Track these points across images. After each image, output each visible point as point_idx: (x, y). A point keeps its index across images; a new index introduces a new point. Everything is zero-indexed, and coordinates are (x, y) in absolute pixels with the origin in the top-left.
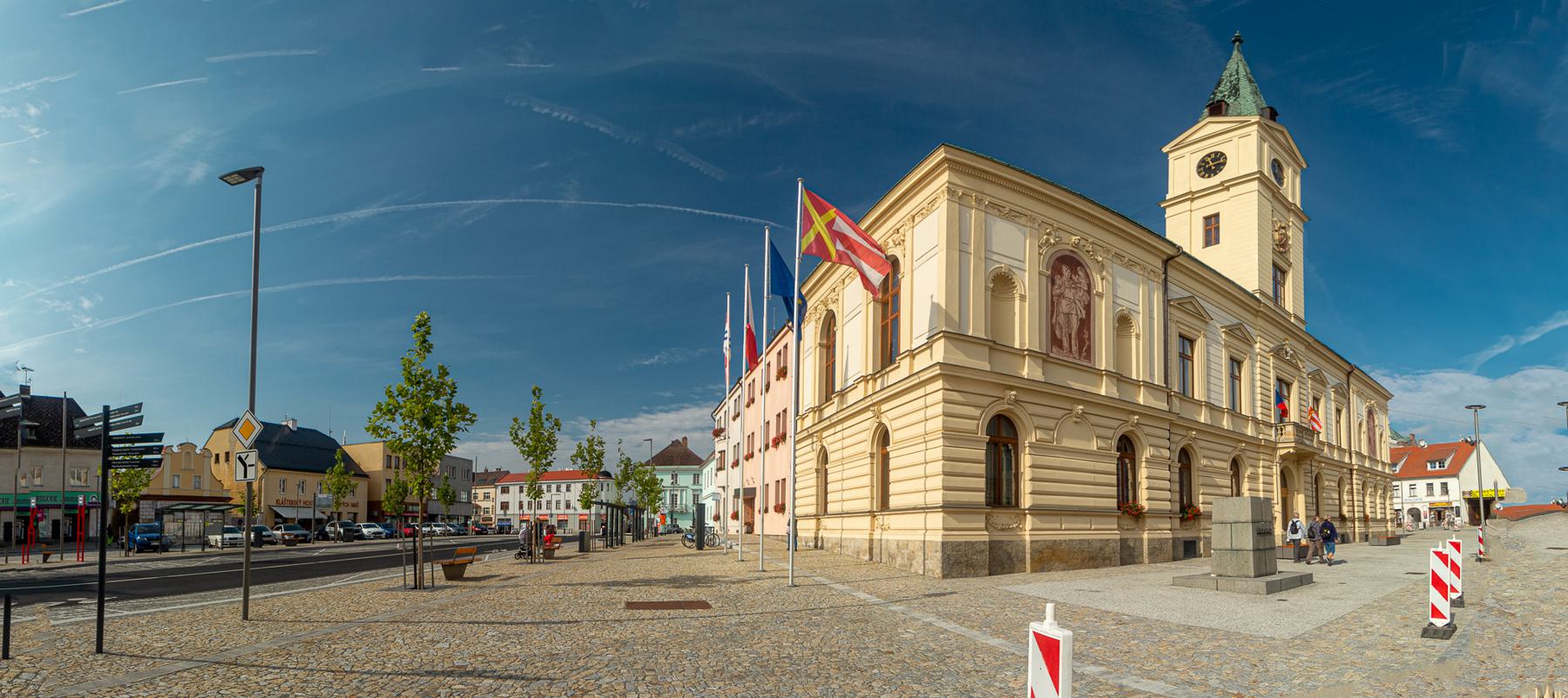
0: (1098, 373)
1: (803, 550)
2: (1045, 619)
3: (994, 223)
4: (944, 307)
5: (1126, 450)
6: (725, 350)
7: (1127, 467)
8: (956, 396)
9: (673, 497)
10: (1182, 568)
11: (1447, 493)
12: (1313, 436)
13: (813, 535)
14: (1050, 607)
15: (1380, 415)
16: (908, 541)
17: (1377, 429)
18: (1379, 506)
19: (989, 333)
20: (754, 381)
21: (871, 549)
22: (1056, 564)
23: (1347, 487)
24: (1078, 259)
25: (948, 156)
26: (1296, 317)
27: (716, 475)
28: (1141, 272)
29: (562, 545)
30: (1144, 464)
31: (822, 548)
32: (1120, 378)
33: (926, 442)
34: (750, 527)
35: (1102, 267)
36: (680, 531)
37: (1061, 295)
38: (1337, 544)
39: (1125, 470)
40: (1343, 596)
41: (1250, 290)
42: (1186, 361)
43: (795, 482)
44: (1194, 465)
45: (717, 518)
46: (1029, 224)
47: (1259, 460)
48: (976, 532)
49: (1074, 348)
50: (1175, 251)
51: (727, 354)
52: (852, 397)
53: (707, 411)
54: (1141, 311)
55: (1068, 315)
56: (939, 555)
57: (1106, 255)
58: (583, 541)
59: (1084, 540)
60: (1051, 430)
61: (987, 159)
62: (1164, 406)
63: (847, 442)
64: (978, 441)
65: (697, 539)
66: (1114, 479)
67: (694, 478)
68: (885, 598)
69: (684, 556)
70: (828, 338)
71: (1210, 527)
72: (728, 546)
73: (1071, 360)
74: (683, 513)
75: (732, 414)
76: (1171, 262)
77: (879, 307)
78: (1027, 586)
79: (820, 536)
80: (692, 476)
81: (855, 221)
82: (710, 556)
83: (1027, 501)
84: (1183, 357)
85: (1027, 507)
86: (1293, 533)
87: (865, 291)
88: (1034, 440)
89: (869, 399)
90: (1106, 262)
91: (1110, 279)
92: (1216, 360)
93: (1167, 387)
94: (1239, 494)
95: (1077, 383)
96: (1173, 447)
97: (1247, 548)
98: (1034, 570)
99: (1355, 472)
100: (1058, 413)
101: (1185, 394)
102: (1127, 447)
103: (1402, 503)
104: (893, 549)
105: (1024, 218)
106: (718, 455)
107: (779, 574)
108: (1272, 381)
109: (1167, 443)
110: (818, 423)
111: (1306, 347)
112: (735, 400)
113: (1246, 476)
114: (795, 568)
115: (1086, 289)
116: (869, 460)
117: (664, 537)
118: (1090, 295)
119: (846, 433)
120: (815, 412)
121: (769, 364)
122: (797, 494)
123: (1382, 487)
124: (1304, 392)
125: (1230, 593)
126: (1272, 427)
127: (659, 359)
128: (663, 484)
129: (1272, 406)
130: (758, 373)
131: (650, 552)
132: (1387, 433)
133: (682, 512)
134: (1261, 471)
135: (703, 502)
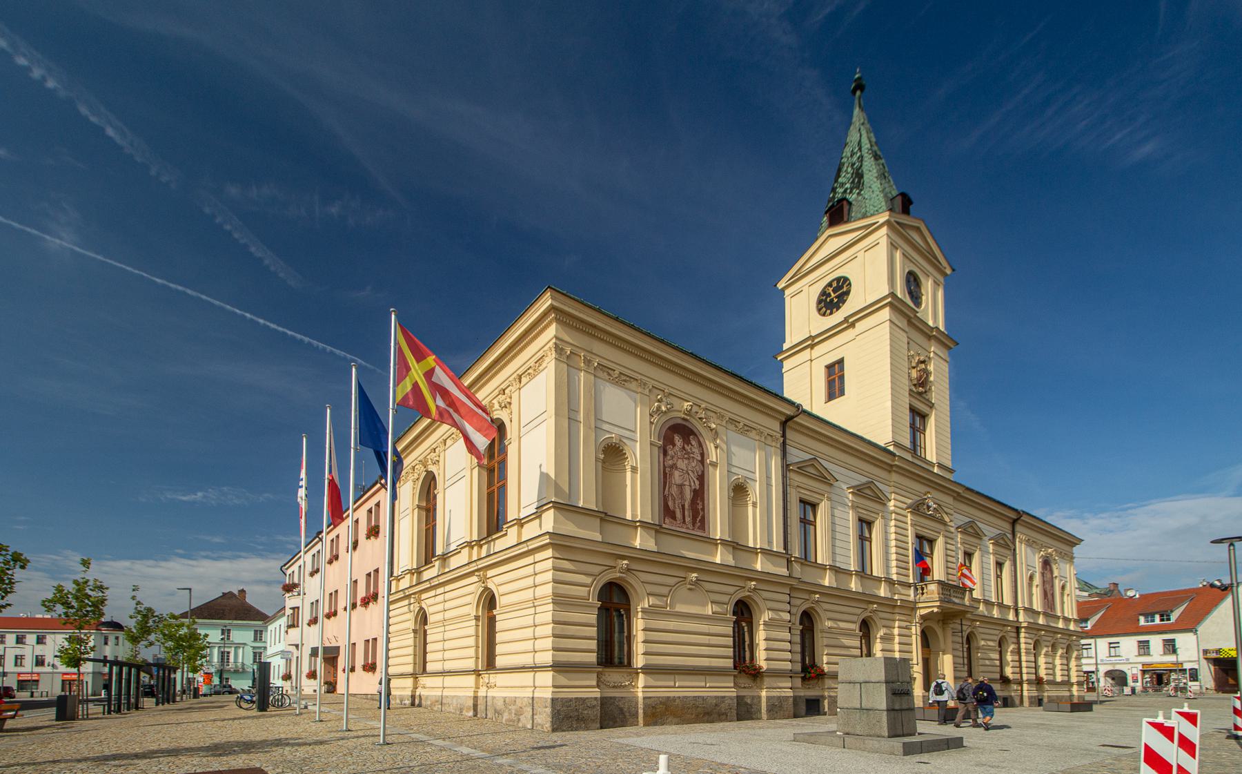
0: (714, 543)
1: (395, 708)
2: (658, 769)
3: (604, 389)
4: (553, 477)
5: (742, 614)
6: (299, 500)
7: (743, 630)
8: (567, 565)
9: (224, 656)
10: (803, 725)
11: (1174, 651)
12: (964, 594)
13: (410, 694)
14: (663, 759)
15: (1061, 564)
16: (516, 698)
17: (1057, 582)
18: (1058, 668)
19: (600, 504)
20: (338, 536)
21: (475, 707)
22: (670, 719)
23: (1012, 647)
24: (690, 426)
25: (555, 304)
26: (940, 466)
27: (287, 632)
28: (757, 438)
29: (20, 713)
30: (762, 627)
31: (420, 705)
32: (736, 546)
33: (535, 607)
34: (331, 687)
35: (715, 434)
36: (232, 691)
37: (674, 467)
38: (997, 707)
39: (741, 633)
40: (1004, 765)
41: (882, 444)
42: (807, 526)
43: (388, 641)
44: (818, 627)
45: (287, 677)
46: (640, 390)
47: (894, 620)
48: (587, 689)
49: (688, 519)
50: (794, 409)
51: (303, 504)
52: (455, 562)
53: (274, 564)
54: (758, 479)
55: (681, 486)
56: (549, 710)
57: (719, 422)
58: (65, 709)
59: (699, 697)
60: (664, 596)
61: (594, 309)
62: (783, 571)
63: (448, 605)
64: (591, 606)
65: (259, 700)
66: (730, 641)
67: (255, 634)
68: (491, 751)
69: (235, 719)
70: (428, 500)
71: (836, 686)
72: (302, 706)
73: (684, 530)
74: (239, 672)
75: (309, 569)
76: (789, 423)
77: (485, 473)
78: (639, 739)
79: (417, 694)
80: (253, 633)
81: (457, 376)
82: (277, 718)
83: (639, 661)
84: (804, 523)
85: (639, 666)
86: (937, 694)
87: (470, 455)
88: (647, 606)
89: (474, 564)
90: (720, 429)
91: (724, 447)
92: (843, 522)
93: (787, 553)
94: (869, 654)
95: (691, 552)
96: (794, 610)
97: (879, 708)
98: (646, 724)
99: (1023, 630)
100: (672, 581)
101: (807, 559)
102: (743, 612)
103: (1096, 664)
104: (500, 704)
105: (634, 383)
106: (289, 612)
107: (368, 733)
108: (910, 539)
109: (788, 607)
110: (416, 585)
111: (955, 498)
112: (314, 555)
113: (878, 636)
114: (387, 726)
115: (699, 458)
116: (474, 622)
117: (209, 699)
118: (703, 466)
119: (448, 596)
120: (413, 574)
121: (357, 521)
122: (391, 654)
123: (1065, 646)
124: (953, 548)
125: (860, 752)
126: (910, 587)
127: (205, 497)
128: (208, 639)
129: (911, 564)
130: (343, 529)
131: (183, 717)
132: (1072, 585)
133: (236, 672)
134: (896, 631)
135: (268, 660)
